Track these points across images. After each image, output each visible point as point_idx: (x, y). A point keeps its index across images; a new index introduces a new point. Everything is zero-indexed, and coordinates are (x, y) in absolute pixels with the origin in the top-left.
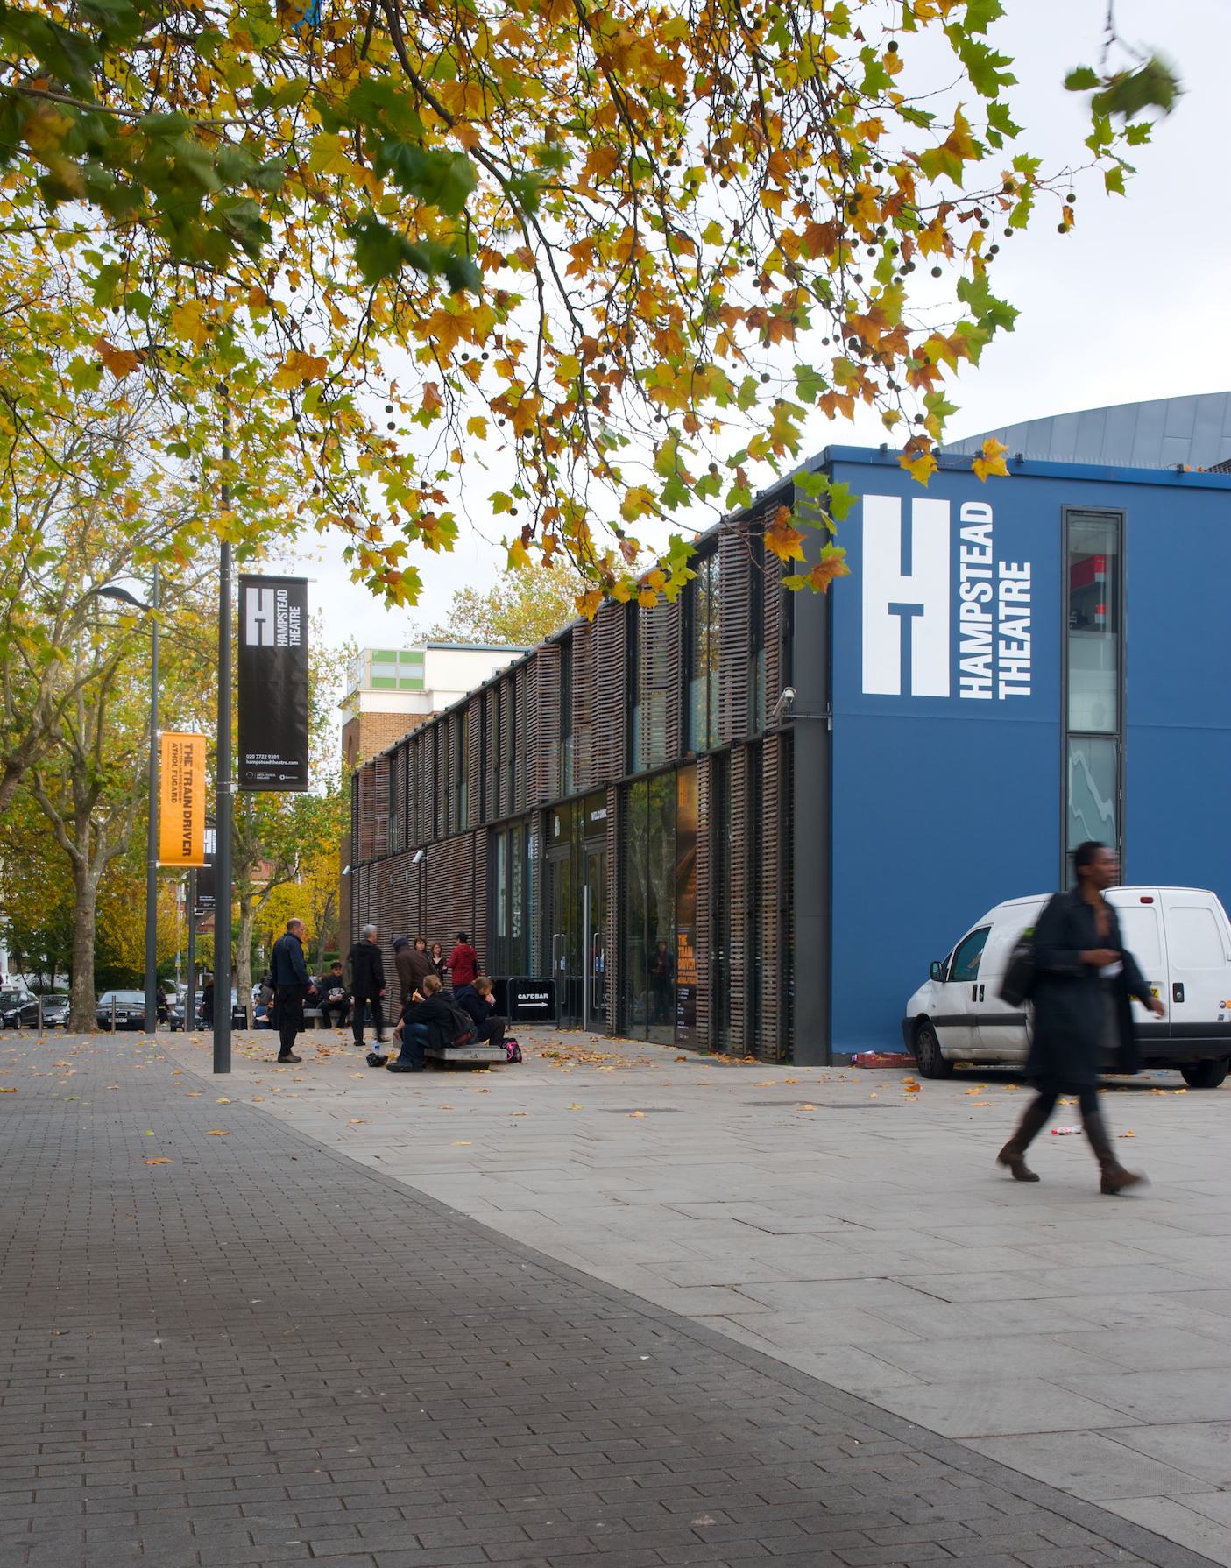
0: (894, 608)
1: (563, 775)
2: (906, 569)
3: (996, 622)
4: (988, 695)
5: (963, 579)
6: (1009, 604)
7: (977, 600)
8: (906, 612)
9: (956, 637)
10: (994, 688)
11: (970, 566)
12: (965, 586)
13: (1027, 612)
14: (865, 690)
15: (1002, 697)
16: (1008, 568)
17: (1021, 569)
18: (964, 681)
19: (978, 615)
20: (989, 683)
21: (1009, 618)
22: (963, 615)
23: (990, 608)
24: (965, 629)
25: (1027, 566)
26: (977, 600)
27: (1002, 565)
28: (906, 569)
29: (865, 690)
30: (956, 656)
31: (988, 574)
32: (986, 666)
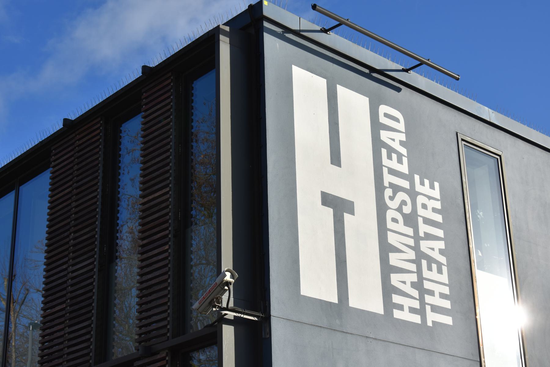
0: (328, 200)
1: (43, 135)
2: (336, 159)
3: (417, 238)
4: (416, 319)
5: (386, 184)
6: (427, 221)
7: (399, 210)
8: (339, 207)
9: (386, 249)
10: (421, 312)
11: (392, 172)
12: (388, 192)
13: (440, 233)
14: (391, 275)
15: (430, 324)
16: (422, 183)
17: (432, 187)
18: (396, 299)
19: (401, 227)
20: (416, 304)
21: (428, 237)
22: (390, 225)
23: (411, 220)
24: (392, 239)
25: (437, 185)
26: (399, 210)
27: (417, 178)
28: (336, 159)
29: (391, 275)
30: (387, 270)
31: (405, 184)
32: (413, 285)
